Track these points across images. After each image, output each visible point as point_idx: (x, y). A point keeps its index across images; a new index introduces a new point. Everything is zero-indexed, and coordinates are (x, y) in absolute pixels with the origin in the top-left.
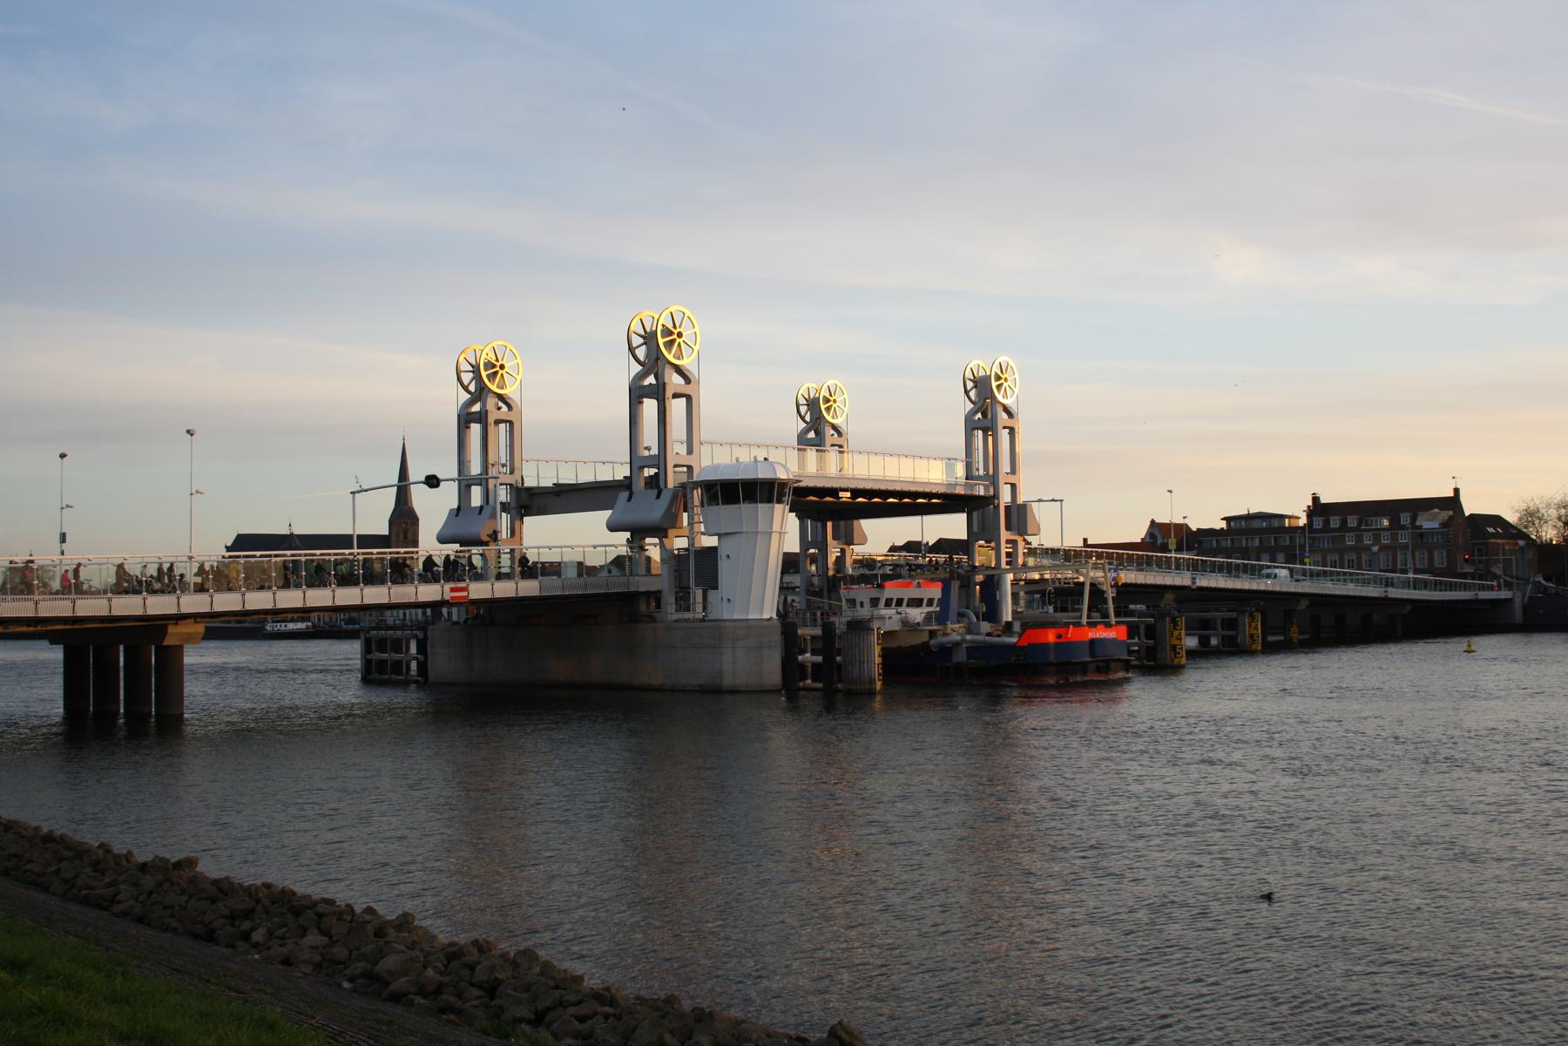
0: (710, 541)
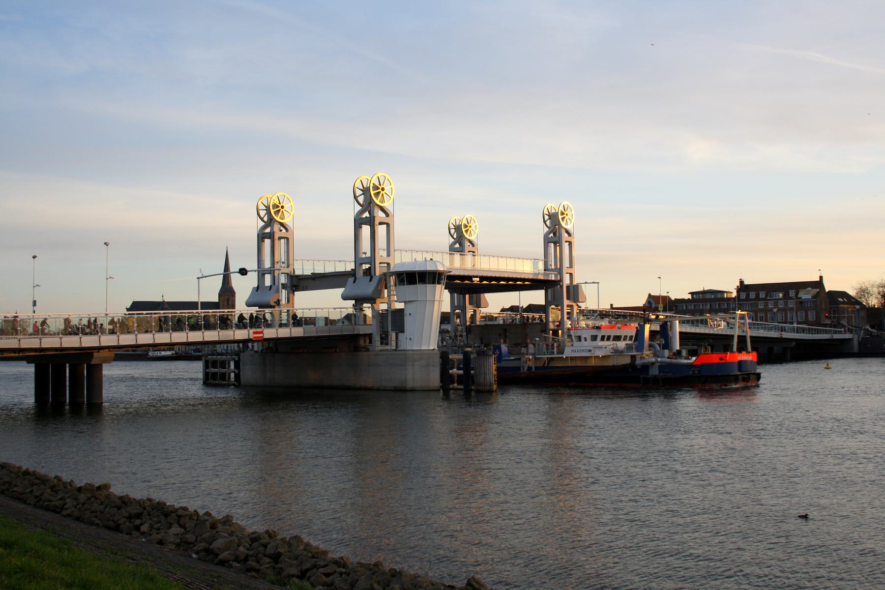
0: (400, 306)
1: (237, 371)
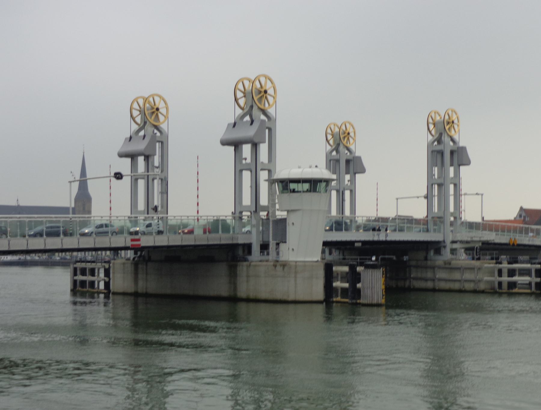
0: (280, 214)
1: (107, 279)
